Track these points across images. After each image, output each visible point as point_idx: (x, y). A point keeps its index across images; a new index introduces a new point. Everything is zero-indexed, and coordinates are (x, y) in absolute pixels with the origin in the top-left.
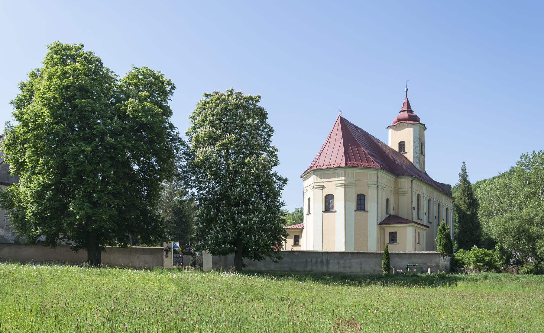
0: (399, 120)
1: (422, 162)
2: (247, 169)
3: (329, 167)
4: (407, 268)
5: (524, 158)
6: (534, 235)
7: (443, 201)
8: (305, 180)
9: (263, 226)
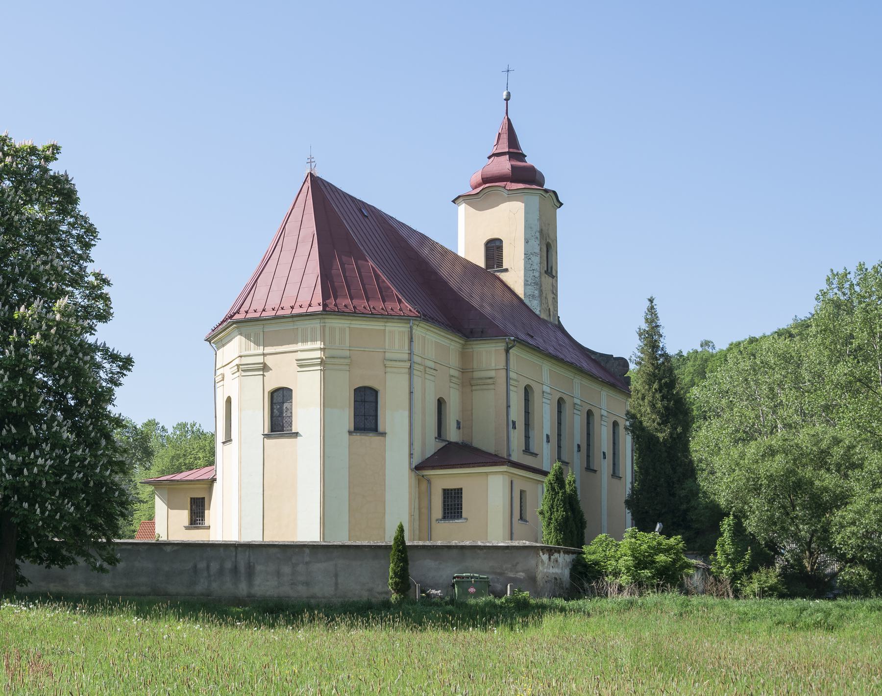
0: (486, 180)
1: (550, 297)
2: (19, 335)
3: (280, 313)
4: (453, 586)
5: (835, 282)
6: (826, 497)
7: (604, 405)
8: (218, 349)
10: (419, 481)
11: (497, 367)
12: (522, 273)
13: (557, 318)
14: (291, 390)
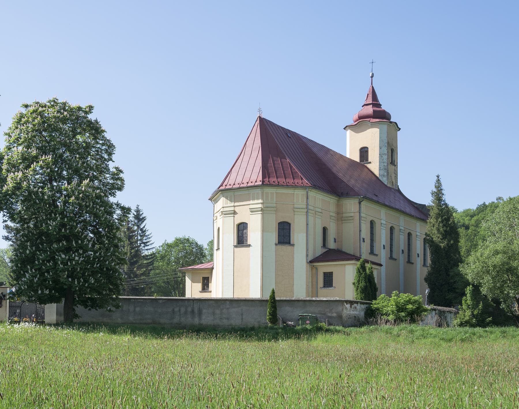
0: (360, 118)
1: (393, 176)
3: (242, 186)
4: (299, 320)
8: (215, 204)
9: (89, 267)
10: (312, 268)
11: (354, 212)
12: (378, 164)
13: (397, 186)
14: (247, 224)
